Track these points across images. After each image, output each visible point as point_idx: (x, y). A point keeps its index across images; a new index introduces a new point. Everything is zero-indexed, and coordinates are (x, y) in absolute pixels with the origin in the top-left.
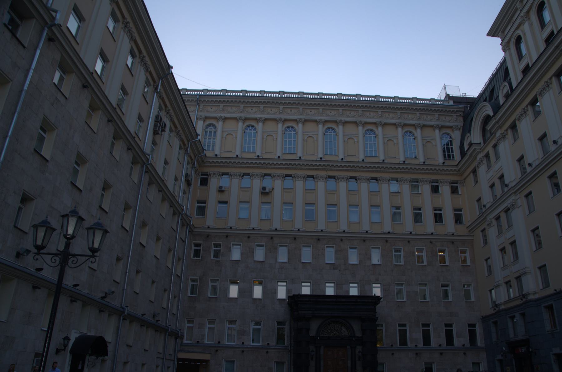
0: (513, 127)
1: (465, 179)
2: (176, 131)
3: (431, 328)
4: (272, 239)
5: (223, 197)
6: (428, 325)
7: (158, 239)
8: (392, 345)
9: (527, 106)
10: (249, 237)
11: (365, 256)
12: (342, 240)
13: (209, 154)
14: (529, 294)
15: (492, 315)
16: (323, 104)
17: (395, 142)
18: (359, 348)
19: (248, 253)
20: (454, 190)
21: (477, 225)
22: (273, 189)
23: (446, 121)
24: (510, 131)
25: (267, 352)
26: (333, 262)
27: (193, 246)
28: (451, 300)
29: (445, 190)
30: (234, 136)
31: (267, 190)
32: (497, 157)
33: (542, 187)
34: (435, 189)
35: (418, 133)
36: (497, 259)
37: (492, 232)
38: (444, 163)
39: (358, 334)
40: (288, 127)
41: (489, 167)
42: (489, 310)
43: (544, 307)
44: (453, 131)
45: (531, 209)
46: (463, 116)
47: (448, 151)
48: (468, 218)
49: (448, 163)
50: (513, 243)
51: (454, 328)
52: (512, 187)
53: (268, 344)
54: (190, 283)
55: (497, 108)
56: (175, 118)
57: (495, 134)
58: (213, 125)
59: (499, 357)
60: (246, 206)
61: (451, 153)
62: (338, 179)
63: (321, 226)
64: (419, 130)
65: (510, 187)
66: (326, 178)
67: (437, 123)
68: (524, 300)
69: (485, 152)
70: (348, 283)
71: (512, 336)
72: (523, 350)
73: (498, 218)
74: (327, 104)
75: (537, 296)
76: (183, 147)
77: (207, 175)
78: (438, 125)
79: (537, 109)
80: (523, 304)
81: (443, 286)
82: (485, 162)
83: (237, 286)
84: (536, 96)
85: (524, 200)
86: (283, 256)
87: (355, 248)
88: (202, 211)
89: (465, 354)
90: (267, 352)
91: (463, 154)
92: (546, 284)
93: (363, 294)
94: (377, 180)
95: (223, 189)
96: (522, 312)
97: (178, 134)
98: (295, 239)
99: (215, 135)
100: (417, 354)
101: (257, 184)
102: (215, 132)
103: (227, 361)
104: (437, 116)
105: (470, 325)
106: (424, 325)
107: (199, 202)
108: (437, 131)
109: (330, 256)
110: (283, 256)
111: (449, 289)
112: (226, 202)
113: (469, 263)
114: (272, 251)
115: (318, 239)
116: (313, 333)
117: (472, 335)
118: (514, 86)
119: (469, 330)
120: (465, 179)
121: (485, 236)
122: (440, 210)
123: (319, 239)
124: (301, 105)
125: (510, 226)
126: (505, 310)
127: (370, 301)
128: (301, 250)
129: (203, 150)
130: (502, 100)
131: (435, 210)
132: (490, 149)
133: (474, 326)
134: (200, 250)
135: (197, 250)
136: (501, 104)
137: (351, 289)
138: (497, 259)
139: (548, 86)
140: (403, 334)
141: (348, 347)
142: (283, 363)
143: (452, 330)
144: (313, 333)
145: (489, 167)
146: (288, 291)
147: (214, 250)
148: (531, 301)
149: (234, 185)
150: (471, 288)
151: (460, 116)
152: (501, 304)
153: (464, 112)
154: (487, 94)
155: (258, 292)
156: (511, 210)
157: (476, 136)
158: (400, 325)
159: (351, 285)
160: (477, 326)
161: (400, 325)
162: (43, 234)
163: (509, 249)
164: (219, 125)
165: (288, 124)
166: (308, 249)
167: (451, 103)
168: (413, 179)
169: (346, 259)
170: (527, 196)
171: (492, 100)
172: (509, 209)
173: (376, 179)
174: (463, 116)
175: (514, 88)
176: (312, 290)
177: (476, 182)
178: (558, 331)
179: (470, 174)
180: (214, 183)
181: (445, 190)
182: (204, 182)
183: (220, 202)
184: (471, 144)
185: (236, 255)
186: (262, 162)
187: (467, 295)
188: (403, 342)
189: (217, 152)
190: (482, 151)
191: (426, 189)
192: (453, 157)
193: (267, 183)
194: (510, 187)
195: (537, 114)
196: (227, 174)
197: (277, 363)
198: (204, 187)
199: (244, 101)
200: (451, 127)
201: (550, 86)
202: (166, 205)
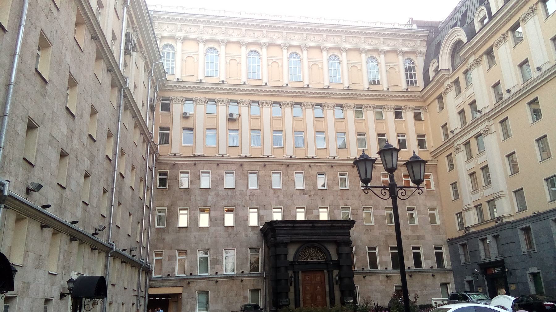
0: (490, 53)
1: (428, 105)
2: (141, 51)
4: (242, 165)
5: (189, 124)
7: (133, 168)
8: (363, 269)
9: (507, 32)
10: (218, 165)
11: (288, 182)
12: (310, 166)
13: (169, 77)
14: (504, 217)
15: (459, 238)
16: (287, 27)
17: (359, 68)
20: (417, 116)
22: (240, 115)
23: (410, 46)
24: (485, 57)
25: (242, 281)
26: (302, 188)
28: (417, 223)
29: (408, 116)
30: (195, 59)
31: (234, 117)
32: (468, 84)
33: (521, 114)
34: (398, 115)
35: (382, 59)
36: (465, 185)
37: (460, 158)
38: (407, 89)
39: (334, 257)
40: (252, 51)
41: (459, 92)
42: (455, 232)
43: (521, 229)
44: (416, 56)
45: (506, 134)
46: (426, 41)
47: (411, 77)
48: (431, 144)
49: (411, 89)
50: (485, 168)
51: (422, 251)
52: (486, 113)
53: (243, 272)
54: (157, 214)
55: (471, 34)
56: (140, 38)
57: (468, 60)
58: (171, 46)
59: (469, 278)
60: (213, 132)
61: (414, 80)
62: (304, 105)
63: (290, 152)
64: (382, 56)
65: (483, 113)
66: (271, 104)
67: (400, 48)
68: (499, 222)
69: (455, 78)
70: (318, 207)
71: (483, 257)
72: (497, 270)
73: (467, 144)
74: (291, 28)
75: (512, 219)
76: (148, 69)
77: (169, 100)
78: (402, 51)
79: (517, 35)
80: (496, 227)
81: (409, 210)
82: (453, 88)
83: (208, 215)
84: (519, 20)
85: (499, 127)
86: (253, 182)
87: (323, 174)
88: (165, 138)
89: (433, 276)
90: (242, 281)
91: (427, 81)
92: (523, 207)
93: (333, 219)
94: (321, 106)
95: (188, 115)
96: (495, 234)
97: (143, 54)
98: (265, 165)
99: (173, 57)
100: (387, 276)
102: (173, 54)
104: (401, 41)
107: (161, 129)
108: (401, 57)
109: (299, 183)
110: (253, 182)
111: (415, 213)
112: (191, 129)
113: (433, 188)
114: (242, 178)
115: (288, 165)
116: (290, 258)
117: (439, 257)
118: (494, 12)
120: (428, 105)
121: (451, 161)
122: (403, 136)
123: (288, 166)
124: (264, 28)
125: (481, 151)
126: (476, 233)
127: (345, 225)
128: (271, 176)
129: (165, 73)
130: (477, 27)
132: (460, 74)
133: (440, 248)
134: (166, 179)
135: (162, 179)
136: (477, 30)
138: (465, 185)
139: (533, 12)
140: (373, 257)
141: (325, 271)
142: (258, 291)
144: (290, 258)
145: (459, 92)
146: (260, 218)
147: (160, 179)
148: (506, 223)
149: (200, 112)
150: (436, 212)
151: (424, 40)
152: (471, 227)
153: (427, 36)
154: (458, 18)
155: (229, 220)
156: (483, 136)
157: (444, 62)
158: (369, 248)
159: (321, 210)
160: (444, 248)
161: (369, 248)
163: (480, 175)
164: (178, 46)
165: (251, 48)
166: (278, 175)
167: (415, 27)
168: (377, 106)
169: (316, 184)
170: (501, 122)
171: (465, 24)
172: (481, 135)
173: (321, 105)
174: (426, 41)
175: (493, 14)
176: (284, 216)
177: (442, 108)
178: (536, 251)
179: (435, 100)
180: (177, 109)
181: (408, 116)
182: (166, 108)
183: (185, 129)
184: (437, 71)
186: (228, 88)
187: (433, 218)
188: (373, 264)
189: (178, 76)
190: (451, 77)
191: (390, 115)
192: (416, 83)
193: (234, 109)
194: (483, 113)
195: (518, 40)
196: (191, 99)
197: (252, 291)
199: (204, 21)
200: (414, 53)
201: (536, 12)
202: (138, 131)
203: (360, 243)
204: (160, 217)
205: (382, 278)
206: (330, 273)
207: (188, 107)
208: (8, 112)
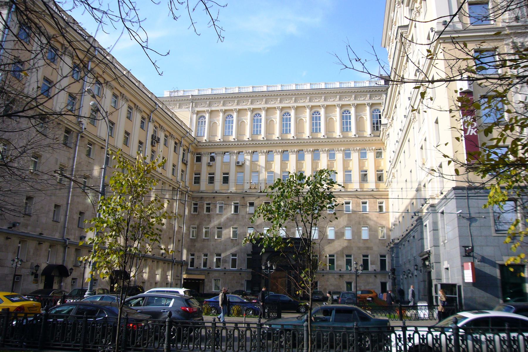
3: (352, 258)
6: (350, 256)
27: (192, 204)
31: (240, 164)
51: (369, 258)
89: (375, 276)
100: (340, 276)
103: (215, 280)
105: (381, 256)
106: (347, 256)
119: (381, 260)
131: (224, 174)
133: (385, 256)
143: (385, 260)
198: (198, 163)
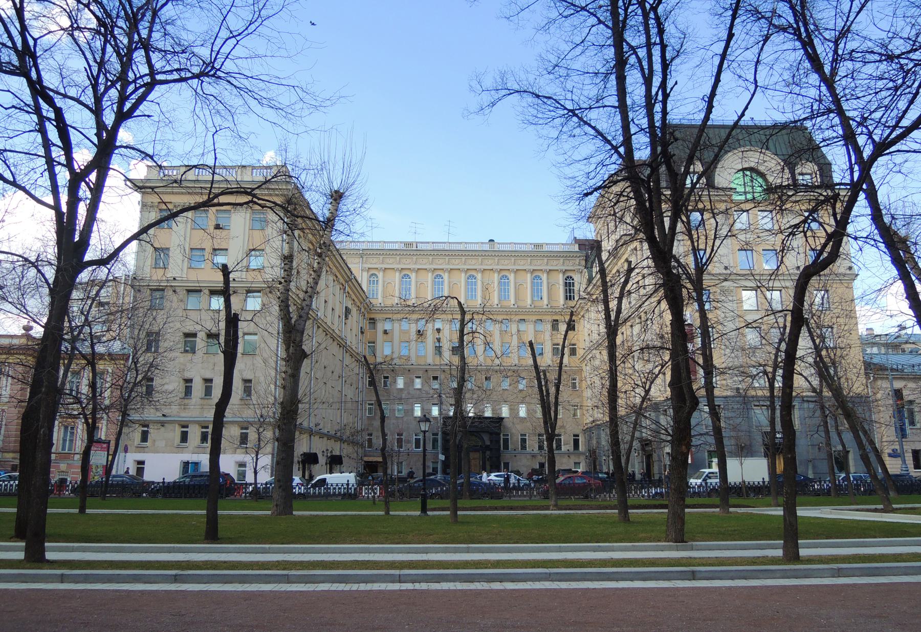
13: (373, 301)
18: (488, 453)
19: (409, 383)
21: (392, 565)
39: (488, 443)
60: (407, 344)
101: (413, 328)
105: (574, 436)
117: (576, 442)
133: (578, 436)
137: (753, 300)
140: (524, 441)
162: (798, 382)
180: (380, 327)
185: (400, 383)
188: (524, 447)
203: (514, 431)
204: (370, 409)
205: (528, 456)
206: (484, 453)
207: (388, 326)
208: (80, 427)
